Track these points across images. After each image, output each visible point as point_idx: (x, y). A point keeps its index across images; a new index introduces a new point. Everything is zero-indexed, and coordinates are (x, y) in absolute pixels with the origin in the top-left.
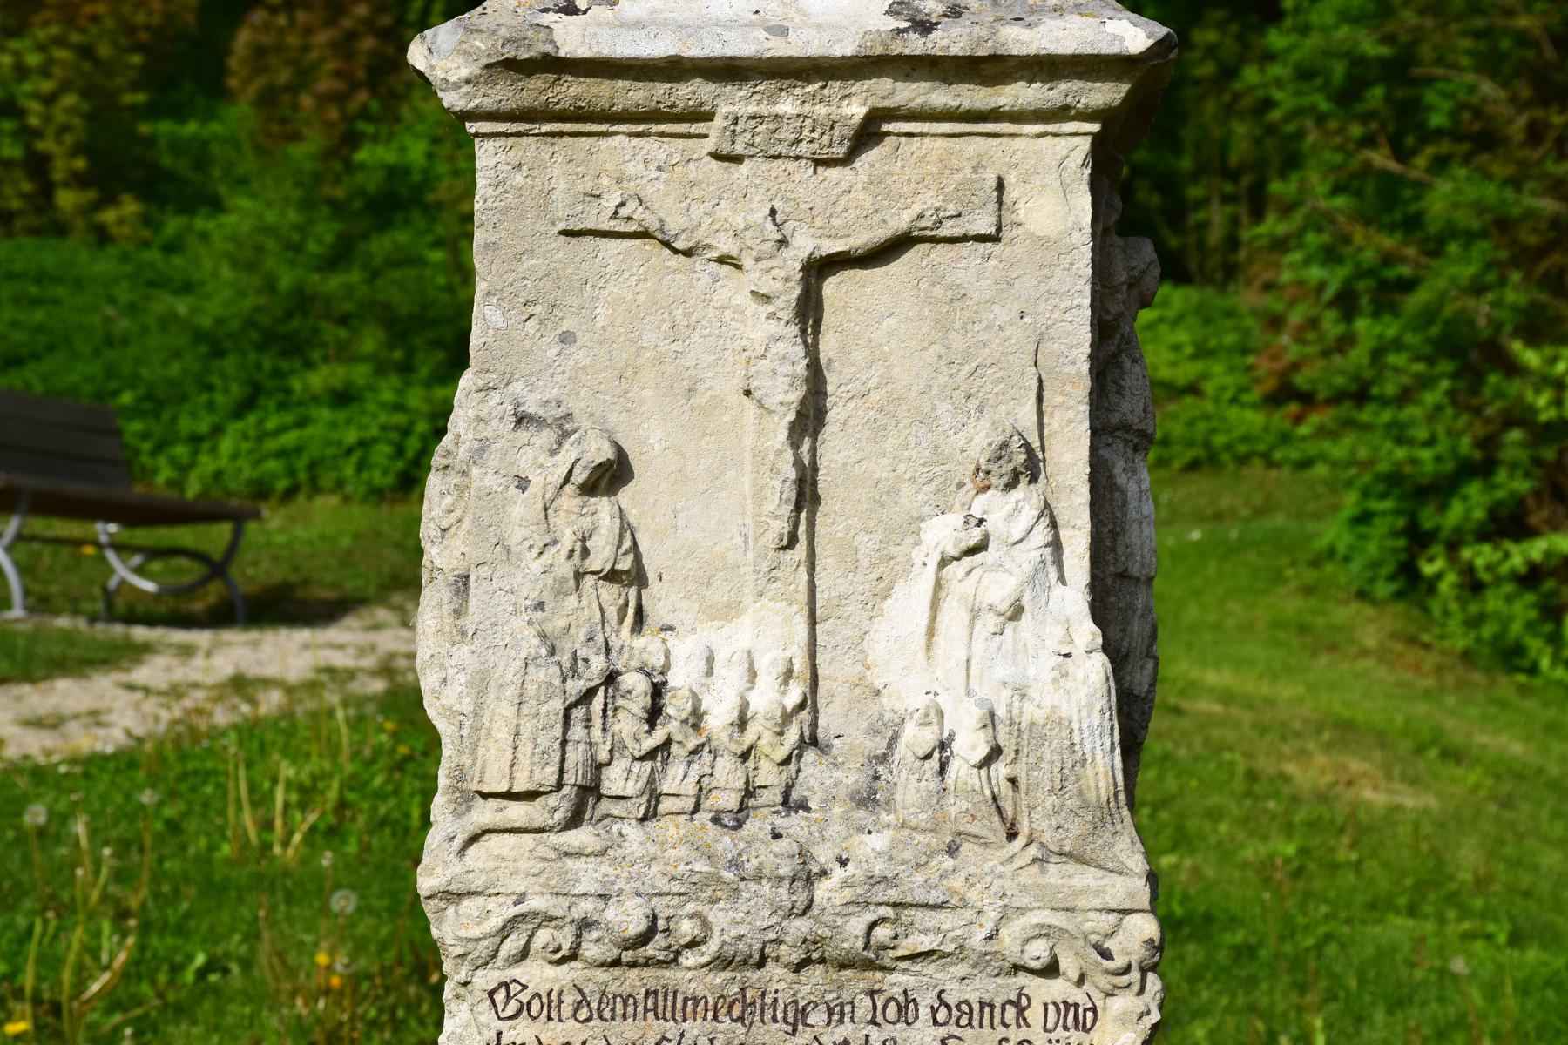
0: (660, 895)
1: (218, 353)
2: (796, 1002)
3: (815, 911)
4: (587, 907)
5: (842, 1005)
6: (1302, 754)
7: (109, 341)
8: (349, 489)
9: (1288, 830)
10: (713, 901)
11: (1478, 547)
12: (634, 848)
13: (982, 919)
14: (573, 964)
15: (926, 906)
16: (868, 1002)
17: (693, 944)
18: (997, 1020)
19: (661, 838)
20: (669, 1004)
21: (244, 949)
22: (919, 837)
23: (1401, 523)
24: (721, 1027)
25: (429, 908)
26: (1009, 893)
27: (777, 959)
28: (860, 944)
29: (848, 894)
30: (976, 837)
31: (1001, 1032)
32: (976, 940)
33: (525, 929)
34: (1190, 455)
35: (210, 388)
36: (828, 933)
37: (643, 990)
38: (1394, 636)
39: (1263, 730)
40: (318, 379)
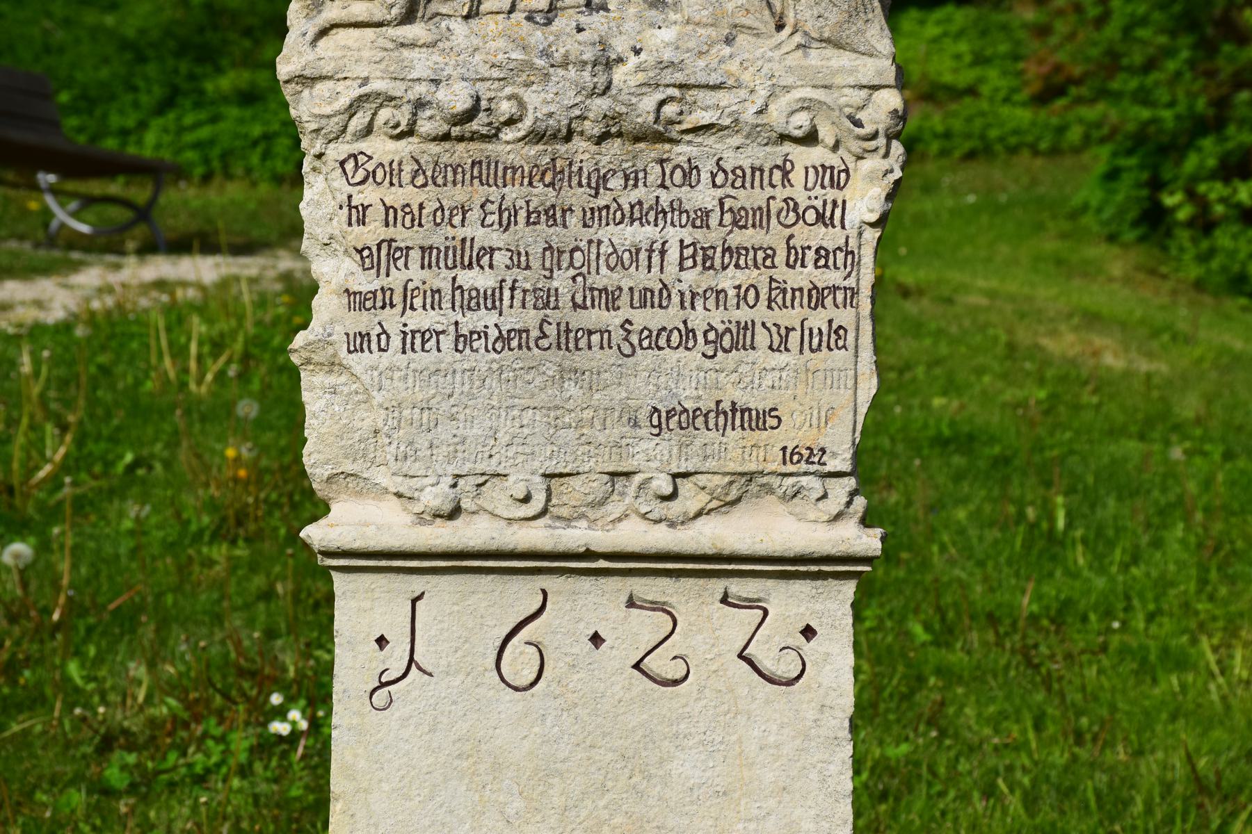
0: (482, 80)
1: (141, 59)
2: (598, 170)
3: (614, 91)
4: (421, 89)
5: (636, 172)
6: (1053, 333)
7: (47, 49)
8: (256, 175)
9: (1041, 382)
10: (528, 85)
11: (1211, 184)
12: (460, 40)
13: (753, 97)
14: (410, 139)
15: (707, 87)
16: (658, 169)
17: (511, 122)
18: (766, 181)
19: (483, 32)
20: (492, 172)
21: (166, 454)
22: (701, 31)
23: (1145, 176)
24: (535, 191)
25: (288, 91)
26: (777, 74)
27: (582, 133)
28: (651, 118)
29: (641, 77)
30: (750, 28)
31: (769, 191)
32: (749, 115)
33: (370, 107)
34: (967, 146)
35: (135, 89)
36: (624, 110)
37: (470, 161)
38: (1138, 268)
39: (1022, 316)
40: (227, 82)
